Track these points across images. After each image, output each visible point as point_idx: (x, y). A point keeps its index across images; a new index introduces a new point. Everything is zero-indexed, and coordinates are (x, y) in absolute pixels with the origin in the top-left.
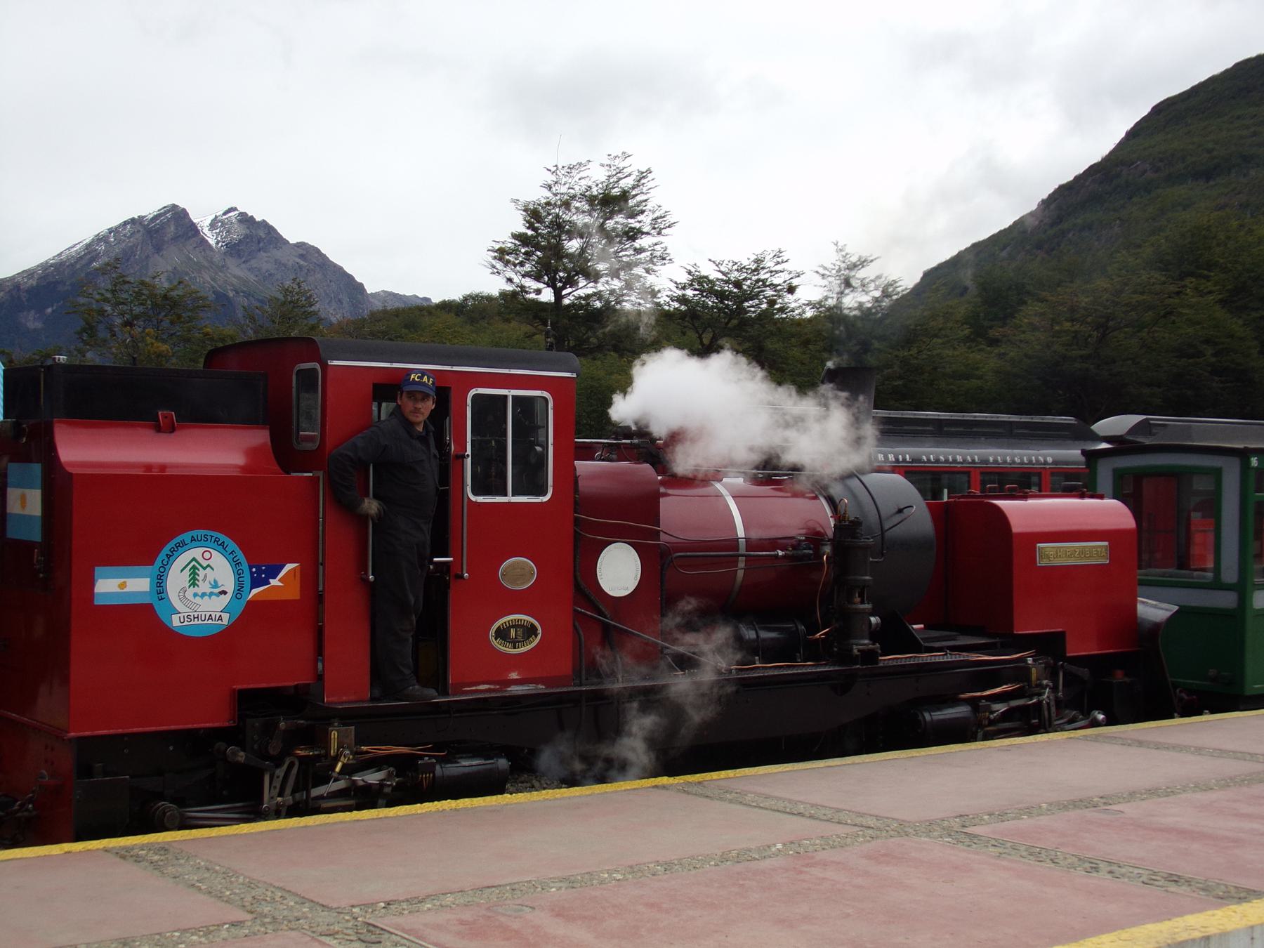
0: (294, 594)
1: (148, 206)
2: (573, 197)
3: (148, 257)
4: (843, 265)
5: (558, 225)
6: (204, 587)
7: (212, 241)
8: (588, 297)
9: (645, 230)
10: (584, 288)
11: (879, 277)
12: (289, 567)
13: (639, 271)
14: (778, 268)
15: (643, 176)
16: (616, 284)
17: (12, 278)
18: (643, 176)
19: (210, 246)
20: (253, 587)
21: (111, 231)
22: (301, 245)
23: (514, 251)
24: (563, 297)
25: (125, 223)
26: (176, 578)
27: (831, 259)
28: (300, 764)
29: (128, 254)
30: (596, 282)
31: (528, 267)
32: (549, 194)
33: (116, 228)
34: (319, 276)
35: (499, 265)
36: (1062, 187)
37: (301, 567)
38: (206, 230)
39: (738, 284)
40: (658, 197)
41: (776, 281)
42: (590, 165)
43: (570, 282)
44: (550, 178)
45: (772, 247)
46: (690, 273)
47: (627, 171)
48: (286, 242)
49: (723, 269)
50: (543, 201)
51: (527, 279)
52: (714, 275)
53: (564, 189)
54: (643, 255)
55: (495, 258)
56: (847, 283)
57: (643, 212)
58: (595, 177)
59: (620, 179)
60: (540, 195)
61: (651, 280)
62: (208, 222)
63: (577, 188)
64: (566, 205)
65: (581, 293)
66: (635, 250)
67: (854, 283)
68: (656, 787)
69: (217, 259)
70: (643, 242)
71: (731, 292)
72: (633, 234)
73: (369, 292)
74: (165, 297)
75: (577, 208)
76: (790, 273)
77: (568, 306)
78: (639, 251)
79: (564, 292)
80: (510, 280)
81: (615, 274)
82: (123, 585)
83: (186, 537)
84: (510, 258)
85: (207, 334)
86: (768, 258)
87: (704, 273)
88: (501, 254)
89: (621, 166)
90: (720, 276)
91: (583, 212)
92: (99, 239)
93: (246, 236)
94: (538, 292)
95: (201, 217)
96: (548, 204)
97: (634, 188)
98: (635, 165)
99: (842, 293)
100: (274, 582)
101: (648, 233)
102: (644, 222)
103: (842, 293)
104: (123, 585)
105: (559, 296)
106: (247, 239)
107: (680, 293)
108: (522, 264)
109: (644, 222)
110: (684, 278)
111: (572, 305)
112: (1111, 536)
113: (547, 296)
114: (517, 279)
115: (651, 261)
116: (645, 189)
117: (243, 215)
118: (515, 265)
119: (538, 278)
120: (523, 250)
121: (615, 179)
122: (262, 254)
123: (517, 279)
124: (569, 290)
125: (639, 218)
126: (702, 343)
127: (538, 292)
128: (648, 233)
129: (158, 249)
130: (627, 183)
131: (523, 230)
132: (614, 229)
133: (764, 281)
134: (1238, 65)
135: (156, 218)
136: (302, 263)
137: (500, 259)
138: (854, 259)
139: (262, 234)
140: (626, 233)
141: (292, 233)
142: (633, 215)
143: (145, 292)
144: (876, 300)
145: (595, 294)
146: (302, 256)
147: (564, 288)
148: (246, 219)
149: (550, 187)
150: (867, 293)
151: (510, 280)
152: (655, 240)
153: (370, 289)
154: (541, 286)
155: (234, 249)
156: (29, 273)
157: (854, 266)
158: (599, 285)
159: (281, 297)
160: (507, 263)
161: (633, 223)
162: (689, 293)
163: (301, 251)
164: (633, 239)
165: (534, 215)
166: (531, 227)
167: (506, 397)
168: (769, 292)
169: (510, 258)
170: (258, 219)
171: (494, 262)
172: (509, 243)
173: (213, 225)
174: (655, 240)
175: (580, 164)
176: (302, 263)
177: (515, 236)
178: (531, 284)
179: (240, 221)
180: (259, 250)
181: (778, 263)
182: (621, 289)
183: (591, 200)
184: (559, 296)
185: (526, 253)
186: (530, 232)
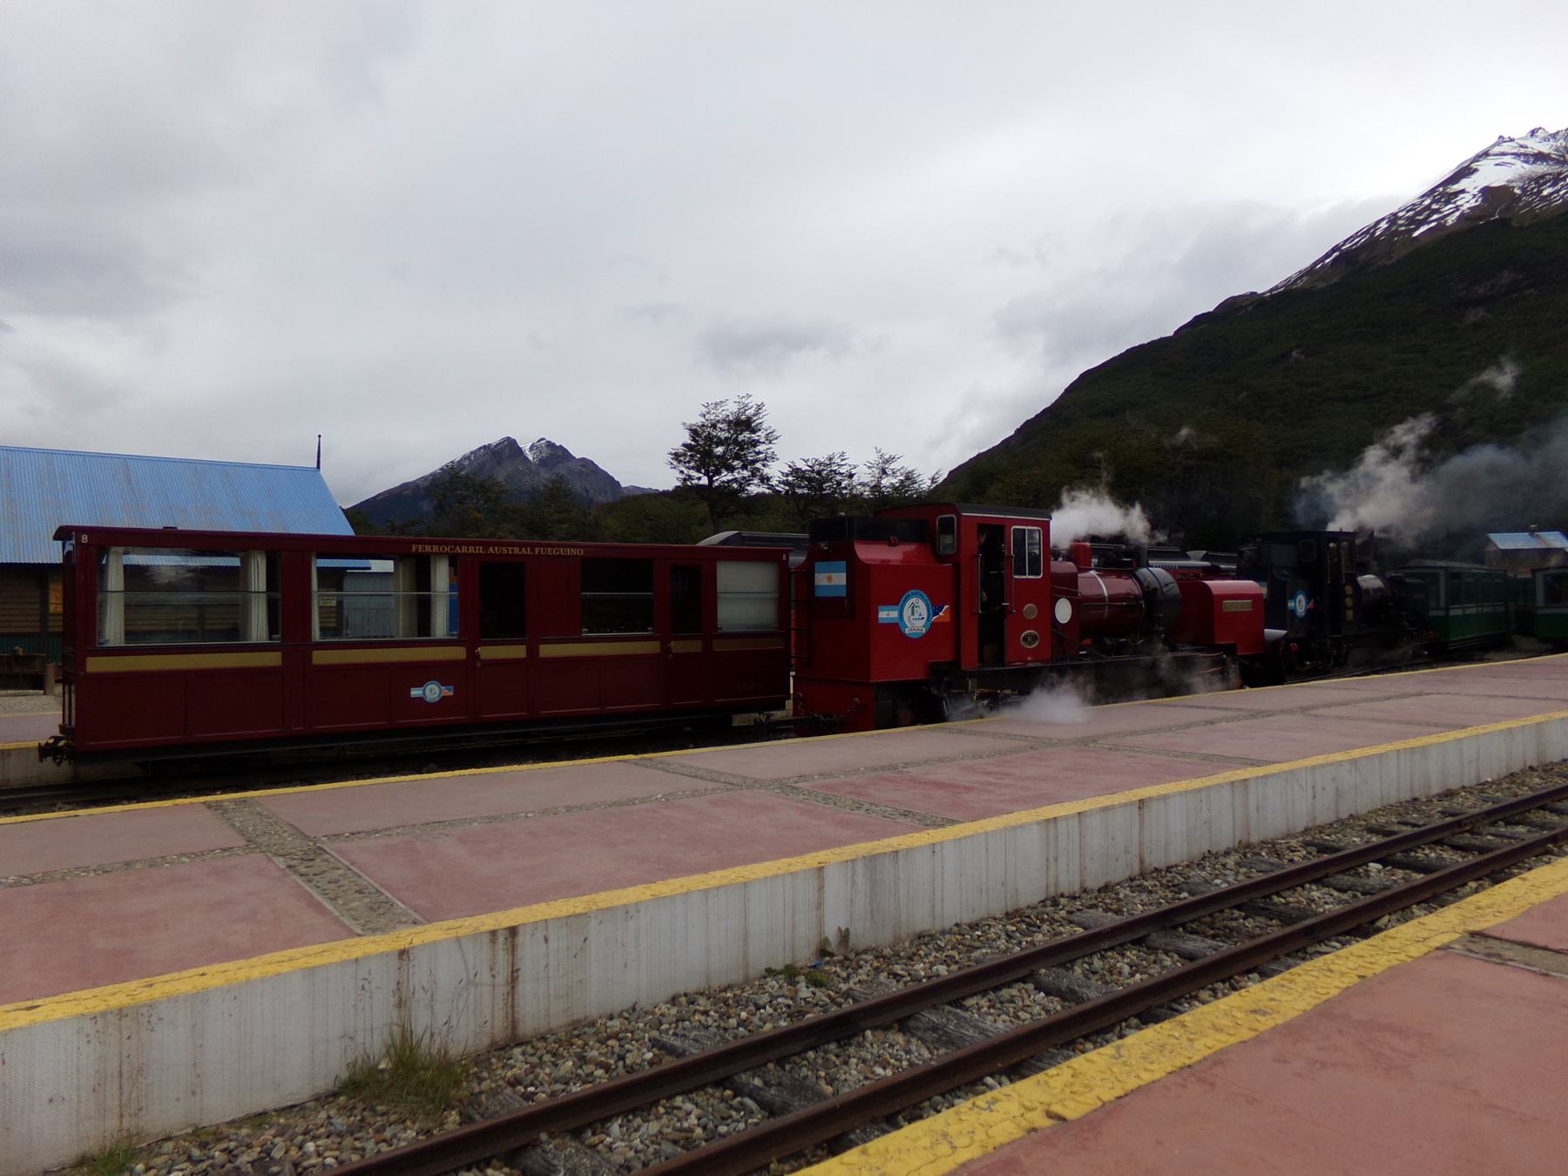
0: (948, 619)
1: (493, 438)
2: (718, 422)
3: (493, 468)
4: (881, 461)
5: (709, 438)
6: (917, 616)
7: (531, 458)
8: (729, 481)
9: (762, 440)
10: (726, 476)
11: (902, 468)
12: (946, 607)
13: (758, 465)
14: (843, 463)
15: (759, 408)
16: (746, 473)
17: (415, 481)
18: (759, 408)
19: (530, 461)
20: (934, 615)
21: (472, 453)
22: (583, 459)
23: (685, 455)
24: (713, 481)
25: (480, 448)
26: (907, 612)
27: (874, 458)
28: (1019, 637)
29: (482, 466)
30: (732, 472)
31: (692, 464)
32: (704, 420)
33: (476, 451)
34: (593, 477)
35: (675, 463)
36: (1028, 421)
37: (950, 608)
38: (527, 452)
39: (819, 473)
40: (768, 421)
41: (841, 471)
42: (728, 402)
43: (718, 472)
44: (704, 410)
45: (838, 451)
46: (790, 467)
47: (750, 405)
48: (575, 458)
49: (810, 464)
50: (700, 424)
51: (692, 471)
52: (805, 468)
53: (712, 417)
54: (761, 456)
55: (673, 459)
56: (884, 472)
57: (760, 430)
58: (731, 409)
59: (746, 410)
60: (700, 420)
61: (766, 471)
62: (528, 447)
63: (720, 416)
64: (714, 426)
65: (725, 479)
66: (756, 452)
67: (890, 472)
68: (619, 761)
69: (534, 468)
70: (760, 448)
71: (815, 478)
72: (755, 443)
73: (623, 486)
74: (481, 486)
75: (720, 428)
76: (850, 466)
77: (717, 487)
78: (759, 453)
79: (714, 479)
80: (682, 472)
81: (744, 467)
82: (888, 615)
83: (910, 593)
84: (682, 458)
85: (506, 507)
86: (836, 457)
87: (798, 466)
88: (676, 456)
89: (746, 402)
90: (809, 469)
91: (724, 430)
92: (465, 458)
93: (550, 455)
94: (699, 479)
95: (525, 445)
96: (703, 426)
97: (754, 415)
98: (754, 401)
99: (881, 478)
100: (941, 614)
101: (763, 443)
102: (761, 435)
103: (881, 478)
104: (888, 615)
105: (711, 481)
106: (551, 457)
107: (785, 479)
108: (689, 462)
109: (761, 435)
110: (787, 470)
111: (719, 486)
112: (1255, 598)
113: (705, 481)
114: (686, 471)
115: (765, 459)
116: (761, 415)
117: (549, 442)
118: (685, 463)
119: (699, 471)
120: (689, 454)
121: (743, 410)
122: (560, 465)
123: (686, 471)
124: (717, 477)
125: (758, 434)
126: (799, 509)
127: (699, 479)
128: (763, 443)
129: (499, 463)
130: (750, 412)
131: (689, 442)
132: (743, 441)
133: (835, 471)
134: (1140, 346)
135: (498, 444)
136: (583, 470)
137: (676, 460)
138: (887, 457)
139: (560, 453)
140: (750, 443)
141: (577, 453)
142: (754, 431)
143: (470, 483)
144: (902, 482)
145: (733, 480)
146: (583, 466)
147: (714, 476)
148: (550, 445)
149: (704, 416)
150: (896, 477)
151: (682, 472)
152: (767, 447)
153: (623, 485)
154: (701, 475)
155: (543, 462)
156: (424, 478)
157: (887, 461)
158: (735, 474)
159: (550, 486)
160: (680, 462)
161: (755, 437)
162: (790, 478)
163: (582, 463)
164: (755, 446)
165: (694, 433)
166: (694, 440)
167: (1029, 575)
168: (838, 478)
169: (682, 458)
170: (558, 444)
171: (672, 461)
172: (681, 450)
173: (531, 449)
174: (767, 447)
175: (722, 402)
176: (583, 470)
177: (684, 445)
178: (694, 473)
179: (547, 446)
180: (558, 462)
181: (842, 460)
182: (749, 476)
183: (730, 422)
184: (711, 481)
185: (690, 456)
186: (693, 443)
